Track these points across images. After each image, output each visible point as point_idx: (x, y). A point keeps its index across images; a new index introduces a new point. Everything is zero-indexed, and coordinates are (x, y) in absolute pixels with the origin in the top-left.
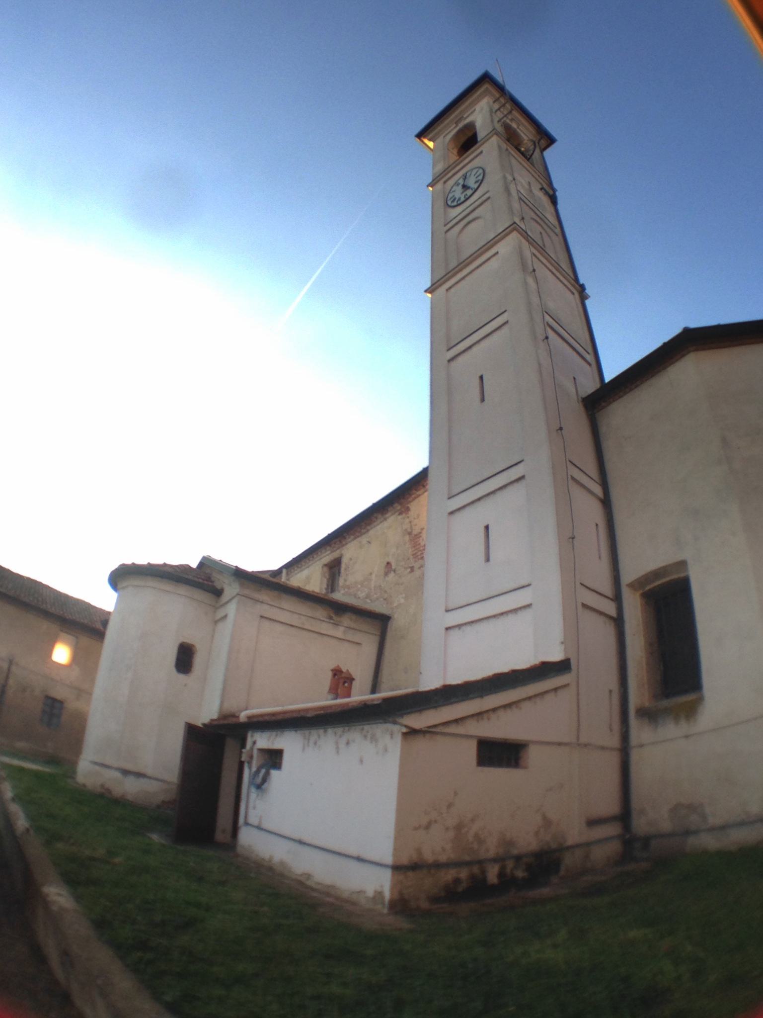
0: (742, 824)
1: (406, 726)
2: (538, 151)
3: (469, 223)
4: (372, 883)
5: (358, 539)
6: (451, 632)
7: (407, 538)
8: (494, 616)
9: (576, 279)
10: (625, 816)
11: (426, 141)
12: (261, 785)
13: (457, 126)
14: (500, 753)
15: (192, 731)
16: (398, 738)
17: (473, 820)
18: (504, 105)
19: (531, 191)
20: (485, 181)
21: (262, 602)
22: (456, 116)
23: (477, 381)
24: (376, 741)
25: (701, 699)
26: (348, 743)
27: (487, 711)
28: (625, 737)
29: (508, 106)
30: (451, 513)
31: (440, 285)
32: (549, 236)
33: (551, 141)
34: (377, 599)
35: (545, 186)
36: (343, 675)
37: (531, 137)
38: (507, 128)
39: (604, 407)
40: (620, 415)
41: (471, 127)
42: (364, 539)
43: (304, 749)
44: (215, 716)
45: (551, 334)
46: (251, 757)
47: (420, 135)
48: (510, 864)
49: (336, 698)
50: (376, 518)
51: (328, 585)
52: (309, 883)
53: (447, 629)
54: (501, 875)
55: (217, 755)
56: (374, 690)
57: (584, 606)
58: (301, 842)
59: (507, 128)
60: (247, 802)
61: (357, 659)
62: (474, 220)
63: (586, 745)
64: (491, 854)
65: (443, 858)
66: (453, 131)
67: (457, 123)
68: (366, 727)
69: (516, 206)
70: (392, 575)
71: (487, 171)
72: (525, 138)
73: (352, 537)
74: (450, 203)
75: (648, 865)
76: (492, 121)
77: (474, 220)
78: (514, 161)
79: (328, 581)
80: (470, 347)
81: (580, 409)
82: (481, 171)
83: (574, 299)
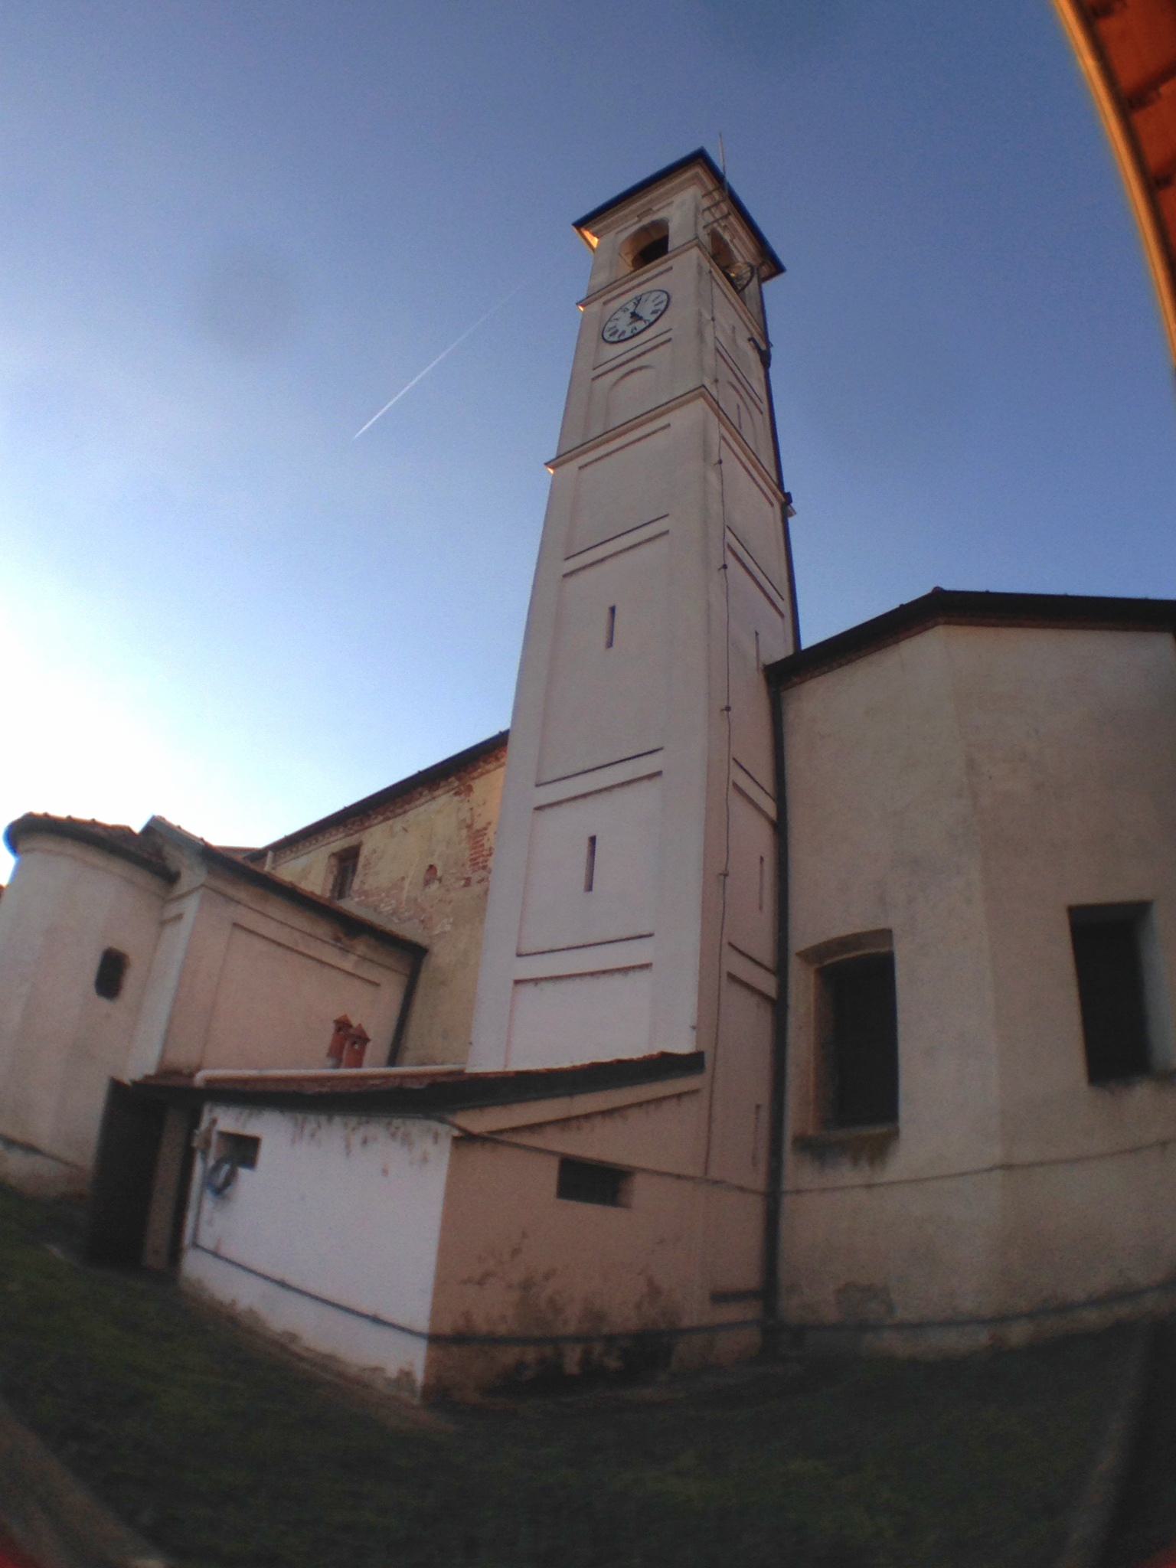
0: (948, 1323)
1: (460, 1128)
2: (755, 280)
3: (632, 371)
4: (402, 1358)
5: (390, 822)
6: (521, 988)
7: (464, 832)
8: (592, 974)
9: (780, 484)
10: (768, 1290)
11: (587, 234)
12: (222, 1190)
14: (592, 1182)
15: (117, 1089)
16: (446, 1144)
17: (547, 1277)
18: (716, 205)
19: (734, 341)
20: (668, 313)
21: (238, 902)
22: (643, 205)
25: (895, 1134)
26: (365, 1142)
27: (577, 1117)
28: (775, 1174)
29: (724, 207)
30: (539, 808)
31: (571, 459)
33: (778, 268)
34: (410, 919)
35: (757, 338)
36: (352, 1031)
37: (749, 260)
38: (716, 237)
39: (794, 685)
40: (816, 701)
41: (661, 226)
42: (398, 824)
43: (293, 1142)
44: (150, 1068)
45: (731, 561)
46: (207, 1143)
47: (581, 224)
48: (598, 1348)
49: (337, 1066)
50: (421, 794)
51: (334, 886)
52: (294, 1347)
53: (517, 982)
54: (585, 1361)
55: (161, 1133)
56: (393, 1059)
57: (732, 977)
58: (283, 1284)
59: (716, 237)
60: (198, 1214)
61: (373, 1009)
62: (640, 368)
63: (716, 1182)
64: (572, 1328)
65: (502, 1329)
66: (632, 226)
67: (640, 217)
68: (397, 1122)
69: (710, 359)
70: (435, 886)
71: (673, 300)
72: (740, 259)
73: (381, 818)
74: (609, 337)
75: (797, 1369)
76: (696, 224)
77: (640, 368)
78: (717, 292)
79: (336, 879)
80: (602, 560)
81: (758, 680)
82: (665, 297)
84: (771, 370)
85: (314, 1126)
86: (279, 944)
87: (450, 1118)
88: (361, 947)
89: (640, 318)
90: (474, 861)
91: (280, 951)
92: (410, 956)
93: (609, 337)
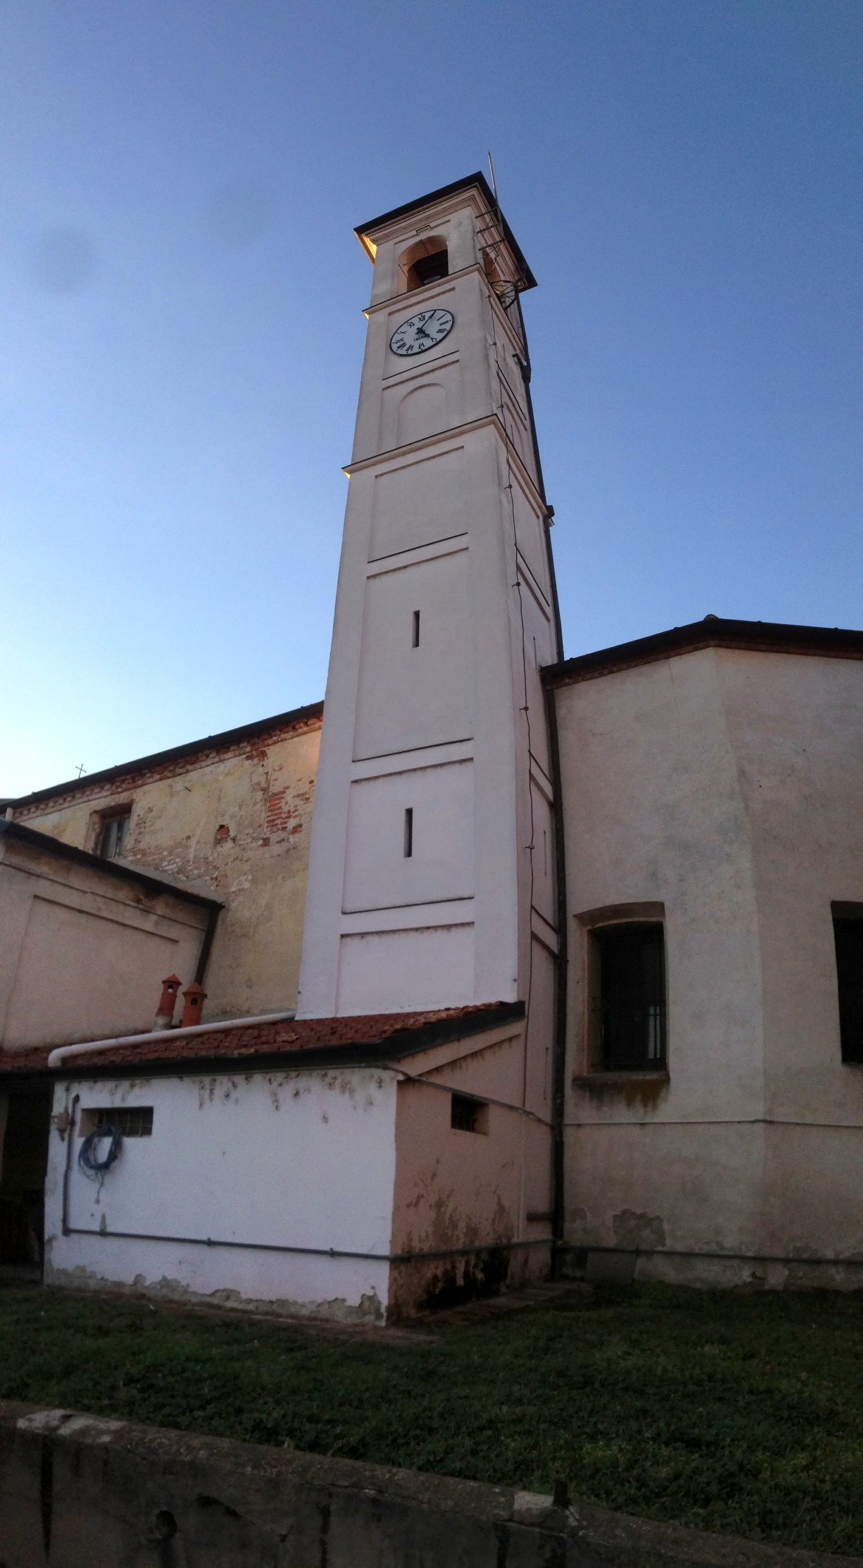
6: (348, 940)
7: (259, 795)
8: (417, 929)
11: (367, 240)
13: (417, 235)
16: (392, 1089)
21: (38, 876)
22: (421, 220)
23: (410, 619)
24: (352, 1091)
30: (356, 782)
32: (519, 431)
33: (532, 283)
42: (179, 783)
50: (207, 756)
53: (343, 936)
62: (429, 385)
67: (419, 232)
68: (332, 1073)
70: (229, 844)
71: (459, 320)
82: (448, 317)
83: (538, 525)
84: (532, 385)
85: (230, 1085)
86: (81, 911)
87: (390, 1064)
88: (161, 907)
89: (428, 336)
90: (271, 823)
91: (83, 919)
92: (207, 913)
93: (396, 349)
